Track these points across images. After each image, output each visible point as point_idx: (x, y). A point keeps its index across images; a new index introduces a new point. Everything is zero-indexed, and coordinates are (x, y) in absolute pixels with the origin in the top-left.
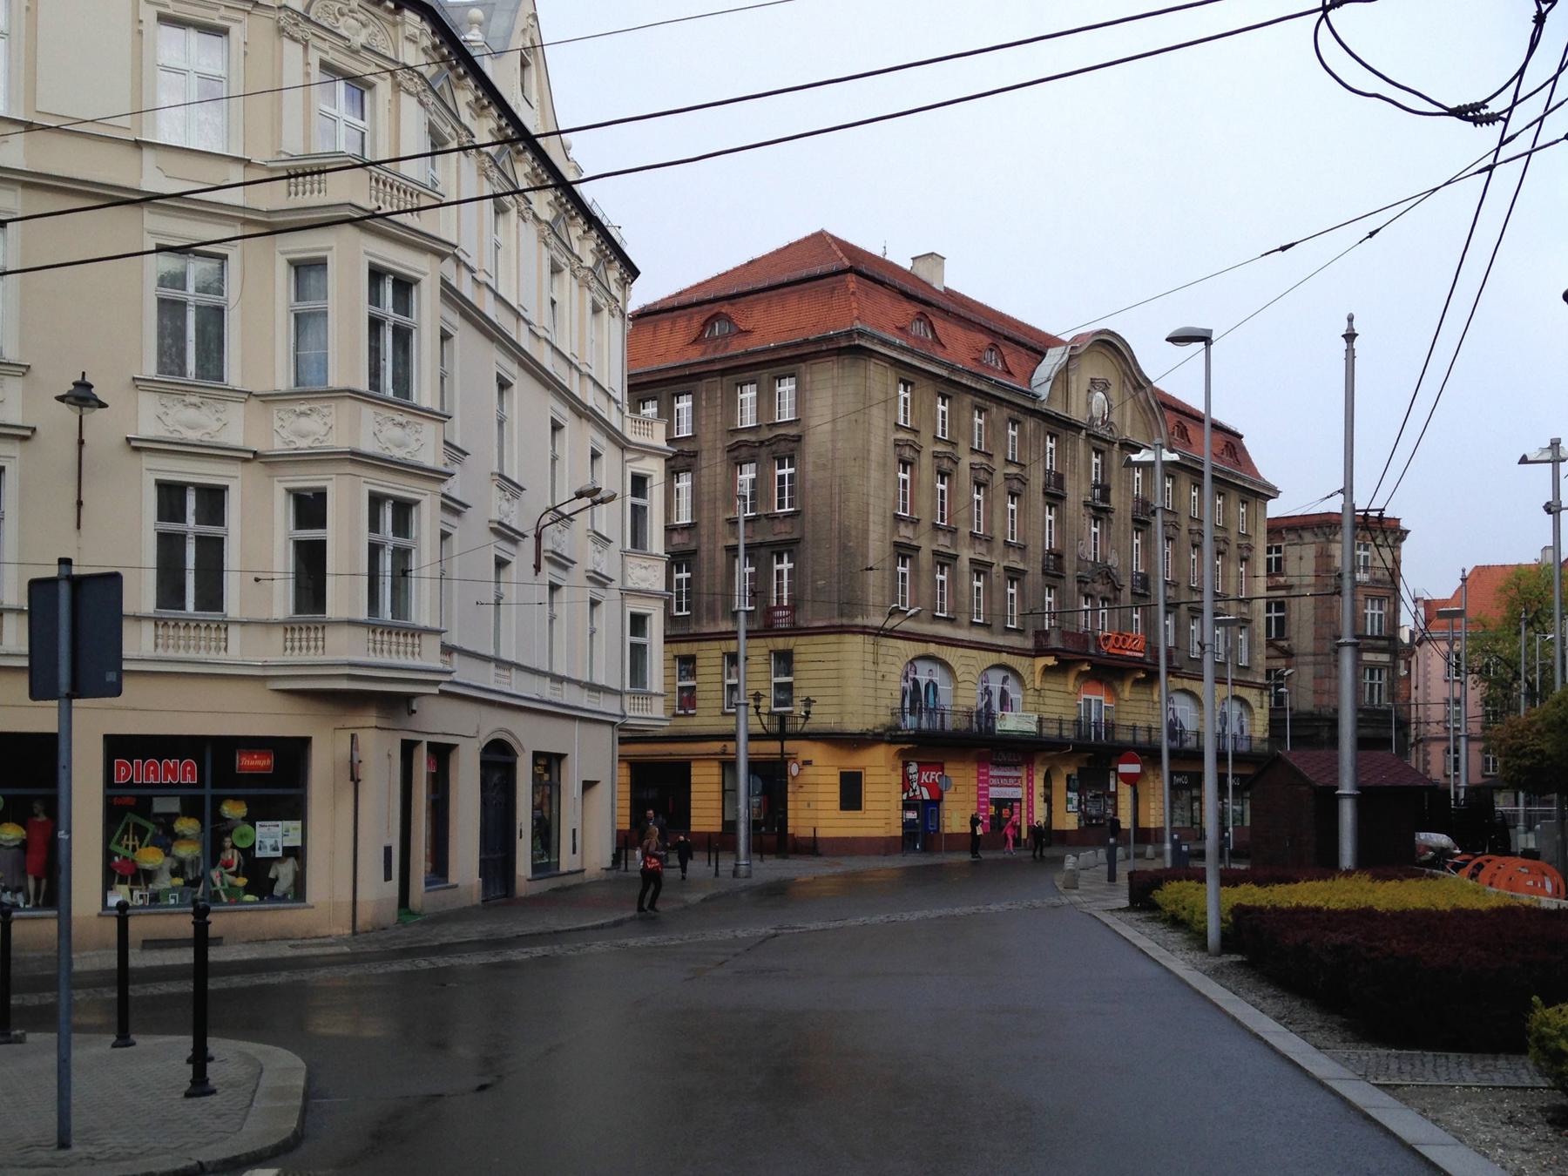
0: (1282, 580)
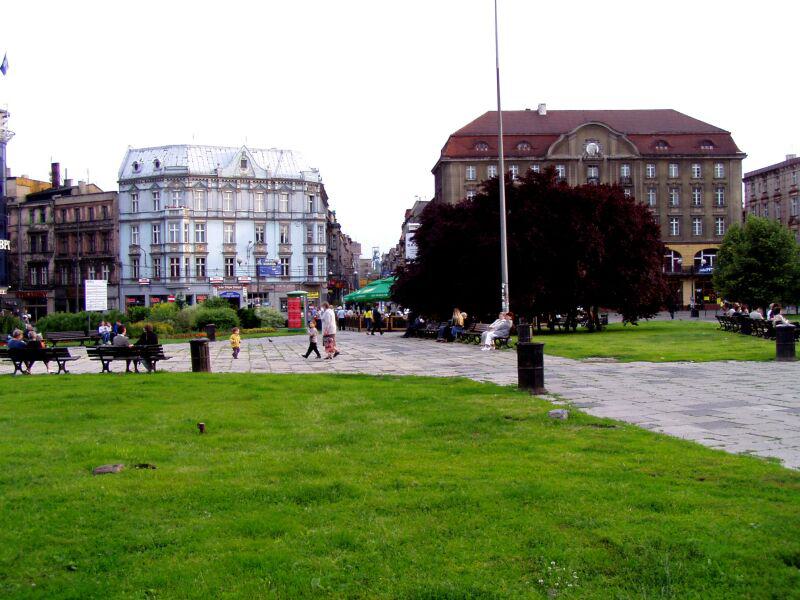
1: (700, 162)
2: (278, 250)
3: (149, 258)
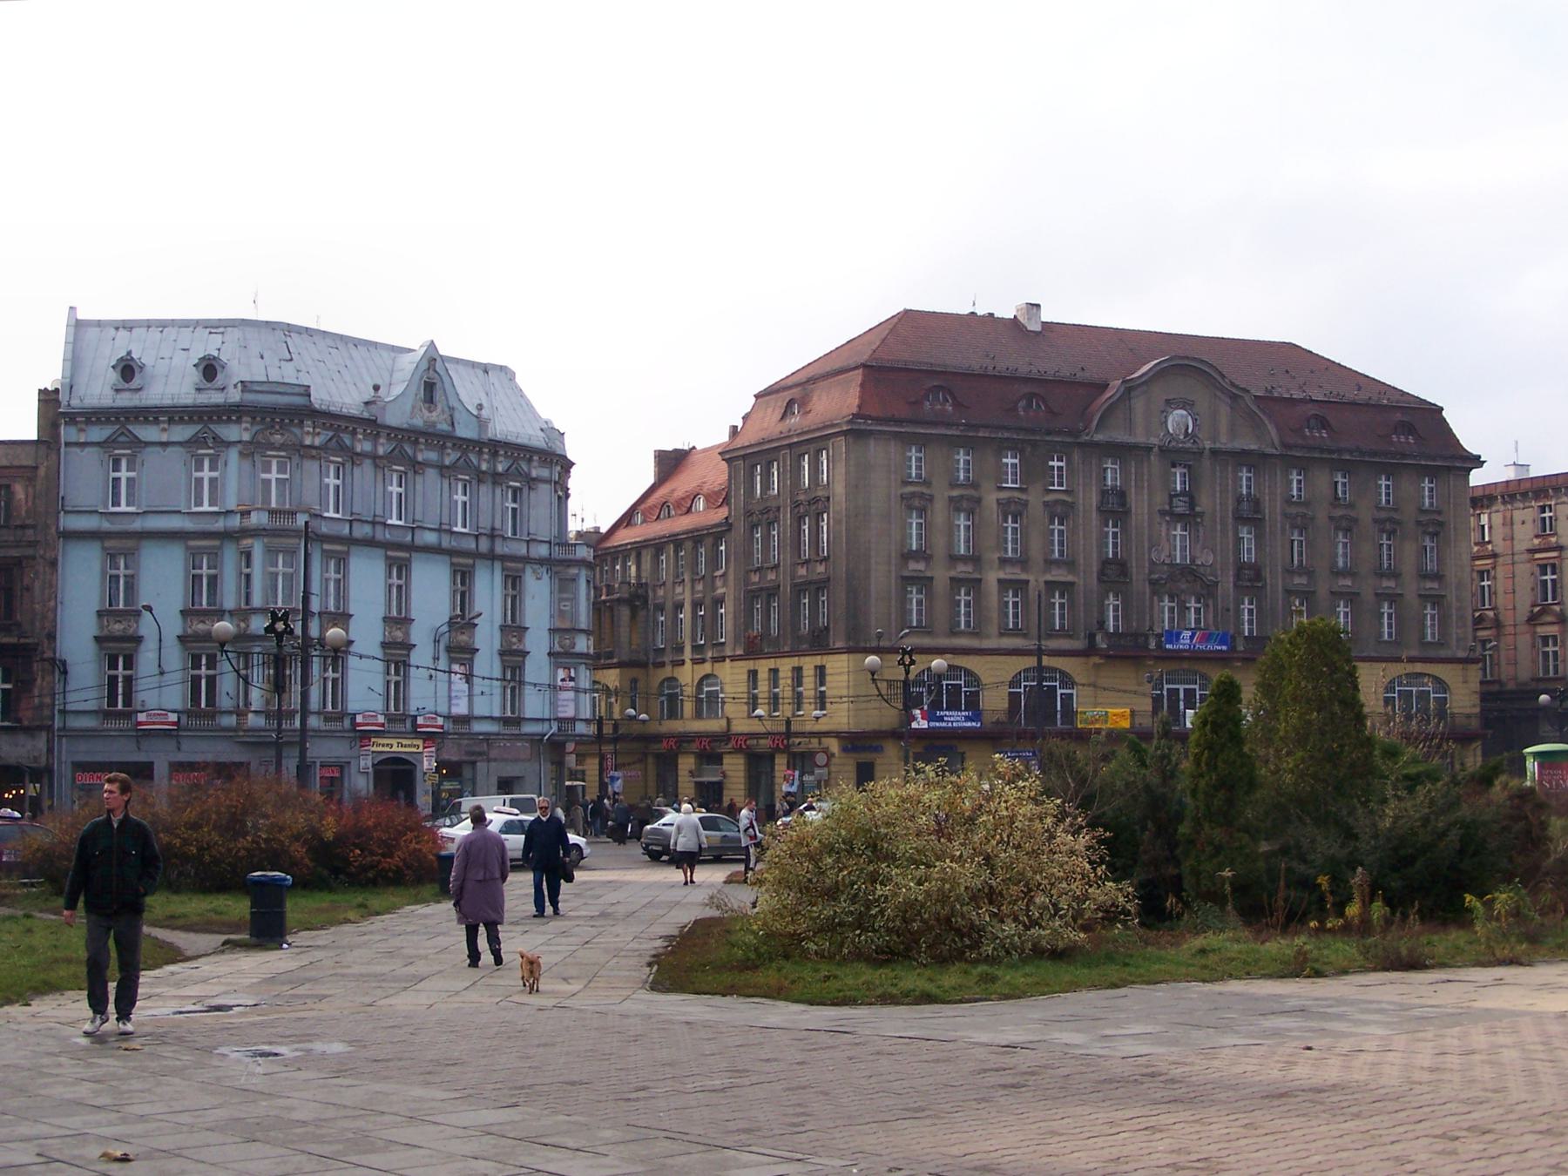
0: (1553, 540)
1: (1391, 470)
2: (497, 645)
3: (175, 658)
